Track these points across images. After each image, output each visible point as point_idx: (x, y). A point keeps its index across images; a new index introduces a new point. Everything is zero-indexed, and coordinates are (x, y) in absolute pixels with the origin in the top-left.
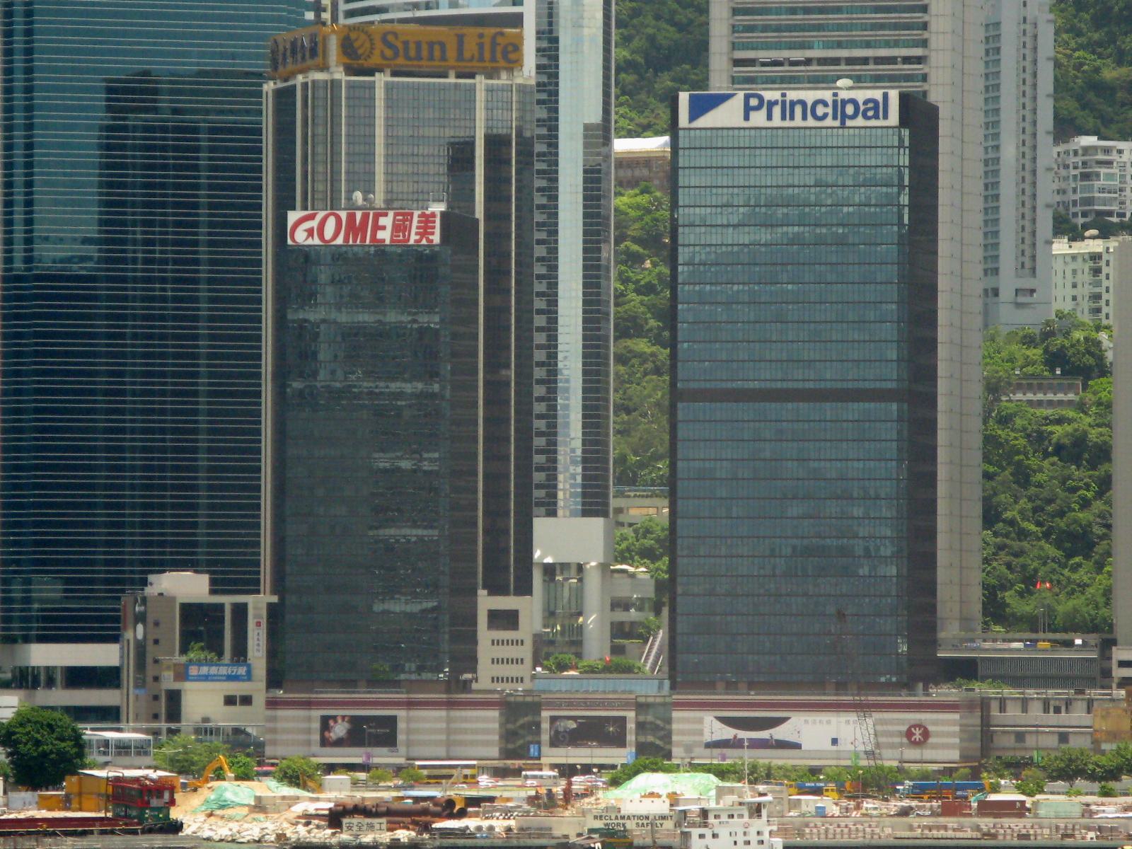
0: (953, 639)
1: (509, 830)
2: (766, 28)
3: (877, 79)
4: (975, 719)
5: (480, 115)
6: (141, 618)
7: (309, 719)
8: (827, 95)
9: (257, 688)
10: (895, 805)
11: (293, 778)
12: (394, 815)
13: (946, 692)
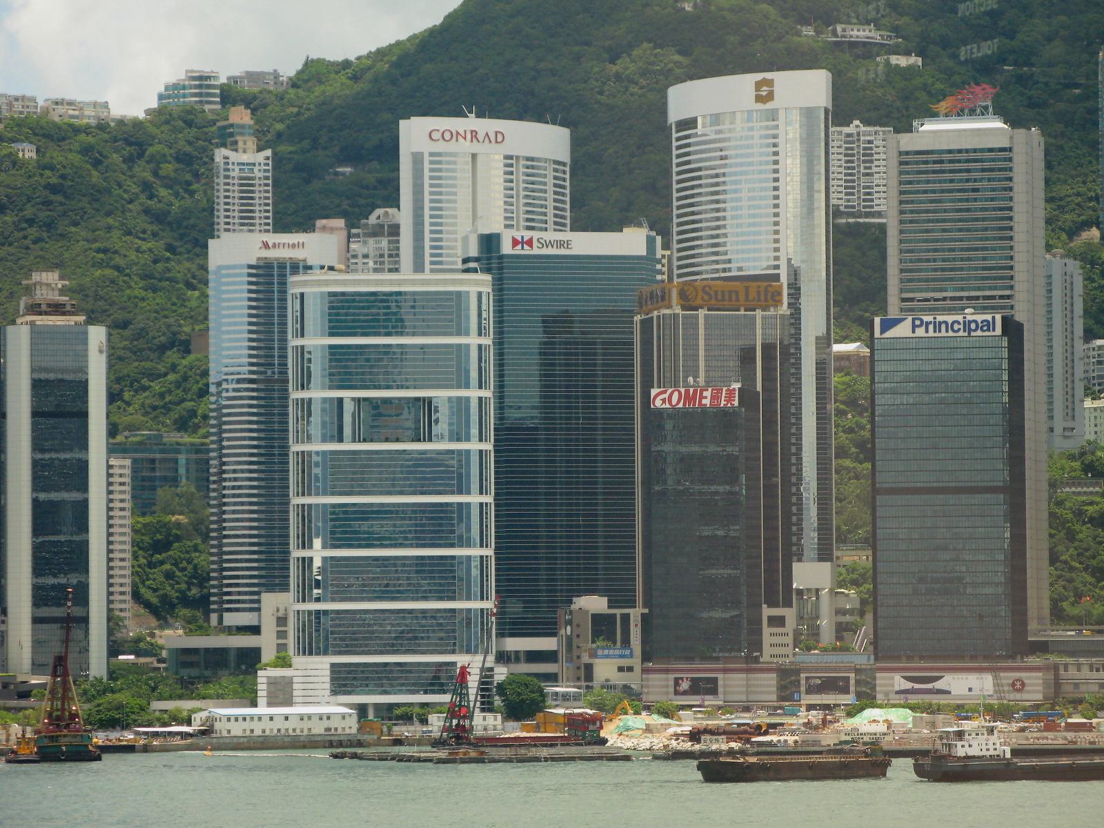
0: (1037, 630)
1: (796, 742)
2: (920, 280)
3: (984, 309)
4: (1051, 676)
5: (759, 332)
6: (569, 622)
7: (667, 680)
8: (960, 318)
9: (636, 662)
10: (1015, 726)
11: (666, 713)
12: (730, 734)
13: (1033, 660)
